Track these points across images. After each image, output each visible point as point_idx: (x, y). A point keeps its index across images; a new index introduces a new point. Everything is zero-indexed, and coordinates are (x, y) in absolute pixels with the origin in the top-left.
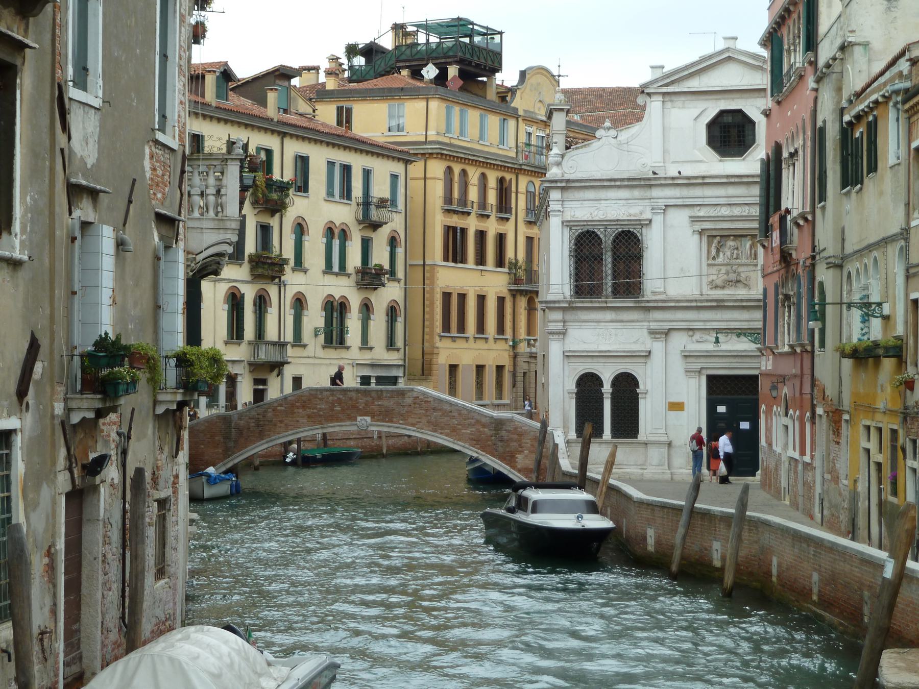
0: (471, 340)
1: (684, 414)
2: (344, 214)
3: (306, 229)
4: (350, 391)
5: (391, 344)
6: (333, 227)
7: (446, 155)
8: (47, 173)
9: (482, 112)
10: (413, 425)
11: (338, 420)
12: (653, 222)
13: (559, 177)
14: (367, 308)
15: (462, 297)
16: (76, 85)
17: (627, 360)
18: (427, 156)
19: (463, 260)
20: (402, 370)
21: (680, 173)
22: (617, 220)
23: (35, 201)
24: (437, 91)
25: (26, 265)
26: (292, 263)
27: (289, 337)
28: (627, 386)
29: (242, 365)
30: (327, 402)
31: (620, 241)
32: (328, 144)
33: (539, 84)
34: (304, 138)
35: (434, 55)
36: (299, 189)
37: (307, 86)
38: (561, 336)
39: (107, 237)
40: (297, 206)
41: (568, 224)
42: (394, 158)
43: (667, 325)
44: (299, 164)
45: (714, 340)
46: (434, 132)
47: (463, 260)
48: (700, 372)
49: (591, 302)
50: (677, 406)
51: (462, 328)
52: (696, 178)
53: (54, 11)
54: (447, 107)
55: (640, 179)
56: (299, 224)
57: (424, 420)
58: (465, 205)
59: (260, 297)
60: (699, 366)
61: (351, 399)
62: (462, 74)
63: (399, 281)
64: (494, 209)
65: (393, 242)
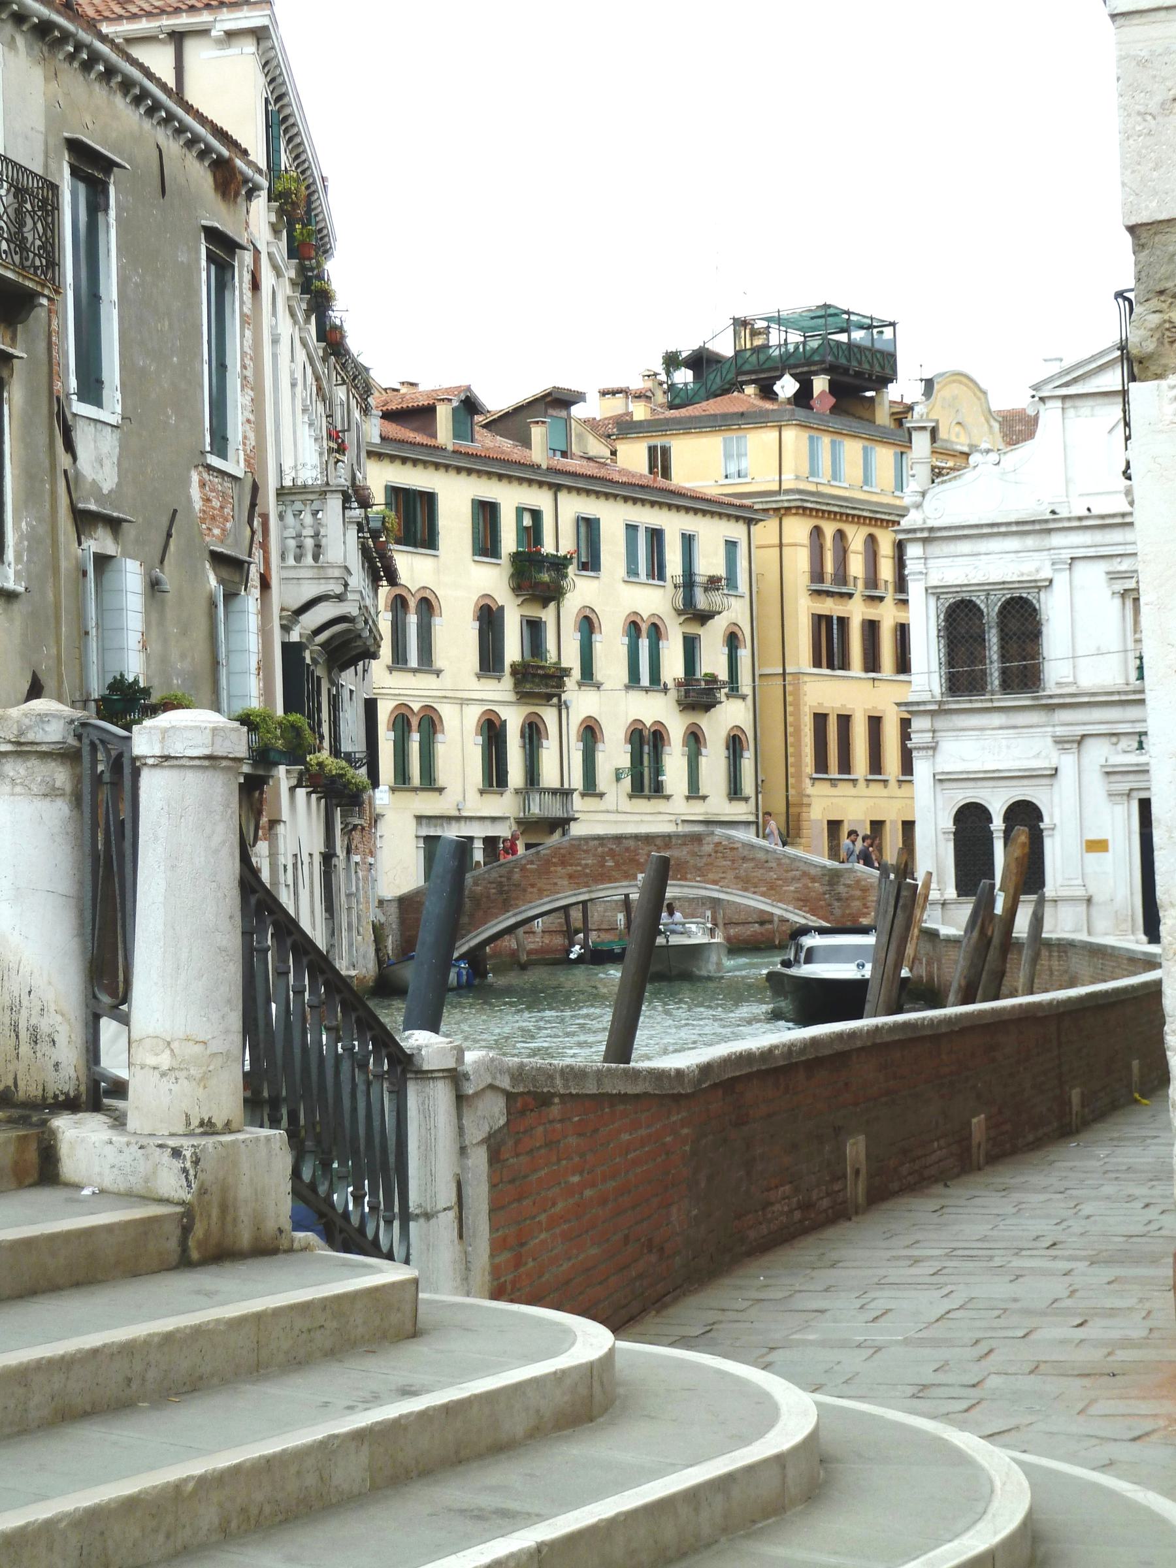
0: (862, 784)
1: (1108, 857)
2: (655, 601)
3: (596, 625)
4: (626, 838)
5: (735, 792)
6: (639, 621)
7: (811, 509)
8: (47, 497)
9: (867, 443)
10: (715, 882)
11: (611, 879)
12: (1055, 583)
13: (919, 524)
14: (695, 738)
15: (845, 721)
16: (81, 399)
17: (1025, 782)
18: (782, 512)
19: (845, 665)
20: (753, 829)
21: (1089, 510)
22: (1004, 583)
23: (33, 528)
24: (793, 415)
25: (23, 598)
26: (576, 674)
27: (576, 780)
28: (1025, 815)
29: (507, 823)
30: (594, 855)
31: (1009, 612)
32: (626, 499)
33: (955, 398)
34: (588, 492)
35: (792, 361)
36: (584, 567)
37: (610, 418)
38: (930, 752)
39: (131, 576)
40: (581, 591)
41: (935, 592)
42: (729, 516)
43: (1080, 730)
44: (583, 530)
45: (1136, 745)
46: (792, 476)
47: (845, 665)
48: (1128, 795)
49: (971, 701)
50: (1097, 846)
51: (845, 765)
52: (1114, 516)
53: (49, 317)
54: (811, 438)
55: (1033, 522)
56: (586, 618)
57: (730, 875)
58: (845, 583)
59: (530, 724)
60: (1126, 787)
61: (627, 849)
62: (834, 388)
63: (744, 698)
64: (891, 588)
65: (732, 640)
